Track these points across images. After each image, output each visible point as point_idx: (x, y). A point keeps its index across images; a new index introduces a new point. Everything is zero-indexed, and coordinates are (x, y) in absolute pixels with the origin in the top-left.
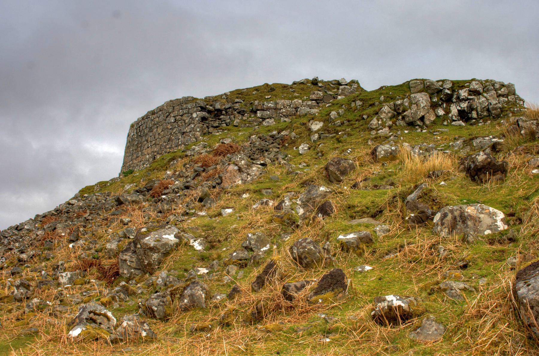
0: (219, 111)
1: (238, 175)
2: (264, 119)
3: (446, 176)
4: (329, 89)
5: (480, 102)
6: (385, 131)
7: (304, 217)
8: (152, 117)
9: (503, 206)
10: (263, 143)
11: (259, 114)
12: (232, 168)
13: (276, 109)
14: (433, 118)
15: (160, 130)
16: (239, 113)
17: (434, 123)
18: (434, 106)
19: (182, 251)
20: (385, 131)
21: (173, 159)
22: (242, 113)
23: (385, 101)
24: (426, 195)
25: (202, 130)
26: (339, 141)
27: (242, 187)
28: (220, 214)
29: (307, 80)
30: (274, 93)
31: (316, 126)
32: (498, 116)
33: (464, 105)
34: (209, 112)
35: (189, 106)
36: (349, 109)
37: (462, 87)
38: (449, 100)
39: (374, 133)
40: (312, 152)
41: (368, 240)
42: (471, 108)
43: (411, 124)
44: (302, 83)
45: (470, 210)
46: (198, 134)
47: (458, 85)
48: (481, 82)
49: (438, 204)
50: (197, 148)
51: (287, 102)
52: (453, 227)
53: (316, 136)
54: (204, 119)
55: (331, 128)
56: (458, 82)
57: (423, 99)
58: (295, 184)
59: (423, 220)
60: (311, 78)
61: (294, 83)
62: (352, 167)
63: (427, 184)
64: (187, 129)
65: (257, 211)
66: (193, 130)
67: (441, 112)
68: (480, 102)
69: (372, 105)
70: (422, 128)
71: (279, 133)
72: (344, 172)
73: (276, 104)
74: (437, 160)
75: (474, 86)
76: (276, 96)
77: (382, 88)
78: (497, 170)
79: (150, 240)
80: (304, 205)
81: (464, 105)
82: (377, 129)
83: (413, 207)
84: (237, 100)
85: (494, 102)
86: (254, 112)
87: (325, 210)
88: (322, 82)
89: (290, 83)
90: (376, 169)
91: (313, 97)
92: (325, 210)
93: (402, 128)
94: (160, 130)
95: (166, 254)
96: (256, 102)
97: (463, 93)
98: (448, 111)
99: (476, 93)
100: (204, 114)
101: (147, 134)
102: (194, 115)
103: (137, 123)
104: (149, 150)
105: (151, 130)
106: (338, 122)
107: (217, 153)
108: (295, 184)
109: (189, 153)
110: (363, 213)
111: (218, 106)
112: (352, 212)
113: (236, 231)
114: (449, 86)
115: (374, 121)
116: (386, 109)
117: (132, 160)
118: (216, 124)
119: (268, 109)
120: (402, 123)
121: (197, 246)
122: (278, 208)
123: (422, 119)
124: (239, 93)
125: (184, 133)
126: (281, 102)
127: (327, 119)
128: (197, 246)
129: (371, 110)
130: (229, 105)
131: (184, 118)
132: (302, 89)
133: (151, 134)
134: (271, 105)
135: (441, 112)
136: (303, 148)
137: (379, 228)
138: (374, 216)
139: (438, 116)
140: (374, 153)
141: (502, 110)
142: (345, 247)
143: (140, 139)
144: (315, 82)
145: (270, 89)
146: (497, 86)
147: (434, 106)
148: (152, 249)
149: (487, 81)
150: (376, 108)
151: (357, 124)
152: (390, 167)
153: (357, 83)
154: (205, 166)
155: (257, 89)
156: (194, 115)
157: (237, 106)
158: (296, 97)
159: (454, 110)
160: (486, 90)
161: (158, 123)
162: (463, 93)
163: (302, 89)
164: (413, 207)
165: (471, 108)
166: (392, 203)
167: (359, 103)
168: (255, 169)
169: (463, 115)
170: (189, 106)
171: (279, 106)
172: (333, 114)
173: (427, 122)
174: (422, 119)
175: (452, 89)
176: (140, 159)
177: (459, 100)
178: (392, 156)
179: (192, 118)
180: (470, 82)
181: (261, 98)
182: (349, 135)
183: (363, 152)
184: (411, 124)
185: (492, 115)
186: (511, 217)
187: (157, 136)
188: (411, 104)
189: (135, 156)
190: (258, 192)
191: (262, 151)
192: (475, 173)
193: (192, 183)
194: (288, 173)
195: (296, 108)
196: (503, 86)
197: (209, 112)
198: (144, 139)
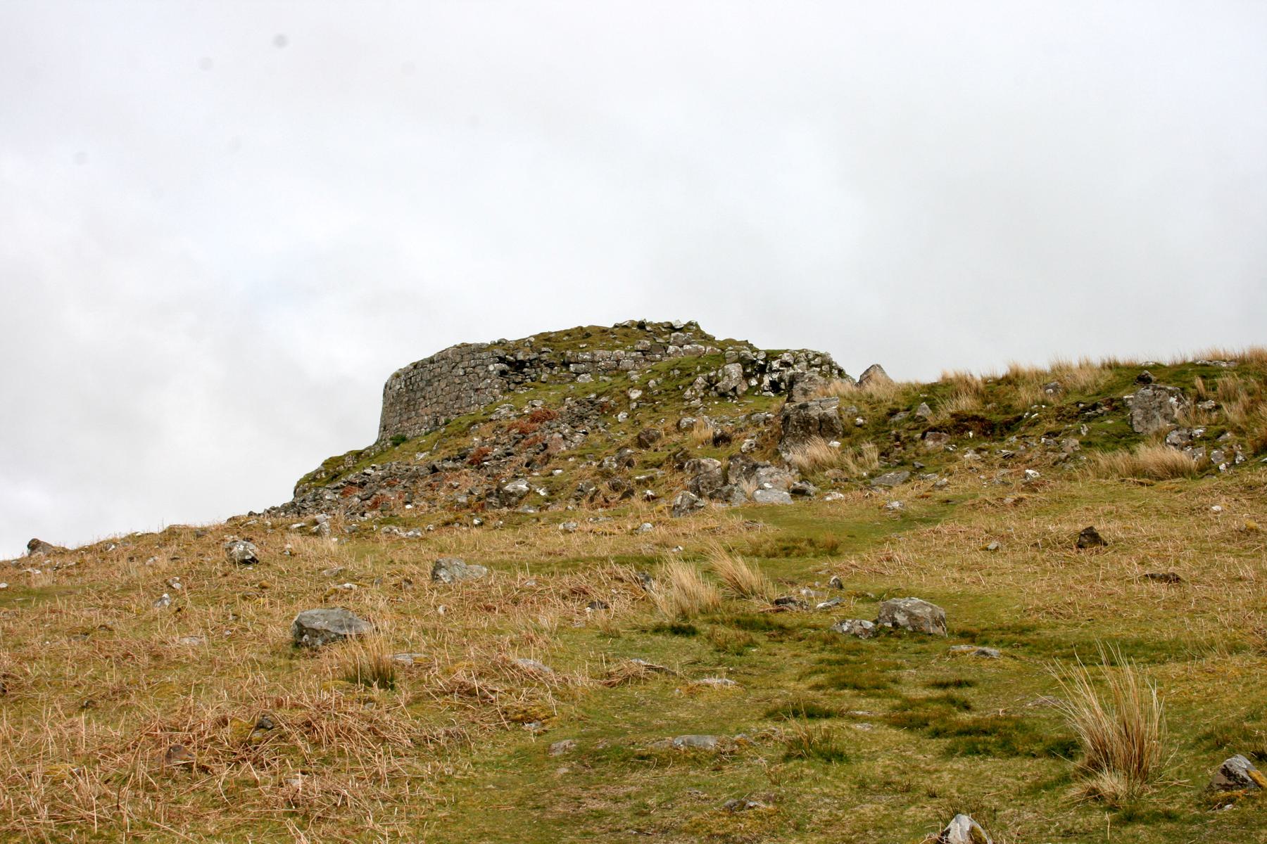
1: (562, 442)
2: (578, 374)
4: (659, 335)
6: (697, 402)
7: (617, 469)
8: (431, 367)
10: (582, 409)
12: (557, 435)
14: (745, 389)
15: (443, 384)
16: (547, 365)
17: (746, 393)
18: (747, 377)
19: (532, 496)
20: (697, 402)
21: (474, 423)
22: (551, 366)
23: (701, 372)
25: (501, 387)
26: (655, 411)
27: (568, 453)
28: (551, 474)
29: (633, 323)
30: (589, 340)
31: (635, 394)
33: (775, 376)
34: (509, 363)
35: (484, 355)
36: (667, 378)
37: (775, 358)
38: (762, 370)
39: (686, 403)
40: (630, 421)
41: (651, 479)
43: (723, 396)
44: (626, 326)
45: (703, 461)
46: (497, 391)
47: (771, 356)
48: (793, 353)
50: (503, 412)
51: (607, 353)
52: (693, 470)
53: (635, 405)
54: (503, 373)
55: (648, 398)
56: (773, 352)
57: (735, 370)
58: (613, 450)
60: (637, 320)
61: (616, 326)
64: (482, 385)
65: (584, 470)
67: (754, 382)
69: (689, 375)
70: (733, 398)
71: (597, 397)
72: (652, 440)
73: (593, 355)
75: (786, 357)
76: (592, 344)
79: (509, 488)
80: (617, 461)
81: (775, 376)
82: (689, 400)
84: (544, 349)
86: (566, 364)
87: (630, 464)
88: (650, 324)
89: (610, 325)
91: (639, 347)
92: (630, 464)
93: (714, 399)
94: (443, 384)
95: (521, 498)
96: (569, 353)
97: (775, 364)
98: (760, 381)
100: (504, 366)
101: (423, 389)
102: (491, 368)
103: (406, 372)
104: (429, 410)
105: (429, 383)
107: (534, 419)
108: (613, 450)
109: (493, 417)
110: (652, 466)
111: (520, 357)
112: (646, 465)
113: (569, 483)
114: (762, 356)
115: (688, 393)
116: (700, 380)
117: (400, 422)
119: (584, 361)
120: (714, 394)
121: (542, 493)
122: (600, 466)
123: (734, 389)
124: (545, 338)
125: (477, 390)
126: (599, 353)
127: (646, 389)
128: (542, 493)
129: (686, 381)
130: (535, 355)
131: (477, 370)
132: (626, 335)
133: (430, 389)
134: (587, 357)
136: (622, 416)
138: (1142, 643)
139: (750, 387)
140: (678, 424)
142: (639, 482)
143: (412, 394)
144: (642, 326)
145: (584, 335)
146: (811, 356)
147: (747, 377)
148: (512, 494)
150: (691, 379)
151: (673, 394)
153: (697, 325)
154: (523, 432)
155: (568, 333)
156: (491, 368)
157: (544, 356)
158: (618, 347)
159: (767, 380)
160: (797, 362)
161: (440, 375)
162: (775, 364)
163: (626, 335)
165: (781, 379)
166: (668, 459)
167: (677, 372)
168: (578, 438)
169: (775, 386)
171: (596, 359)
172: (652, 383)
173: (739, 393)
175: (766, 360)
176: (413, 421)
177: (772, 371)
180: (782, 352)
181: (574, 347)
182: (665, 405)
183: (670, 424)
187: (439, 392)
188: (724, 375)
189: (405, 417)
190: (583, 456)
191: (582, 418)
193: (513, 450)
194: (608, 441)
195: (618, 361)
196: (817, 355)
197: (509, 363)
198: (419, 394)
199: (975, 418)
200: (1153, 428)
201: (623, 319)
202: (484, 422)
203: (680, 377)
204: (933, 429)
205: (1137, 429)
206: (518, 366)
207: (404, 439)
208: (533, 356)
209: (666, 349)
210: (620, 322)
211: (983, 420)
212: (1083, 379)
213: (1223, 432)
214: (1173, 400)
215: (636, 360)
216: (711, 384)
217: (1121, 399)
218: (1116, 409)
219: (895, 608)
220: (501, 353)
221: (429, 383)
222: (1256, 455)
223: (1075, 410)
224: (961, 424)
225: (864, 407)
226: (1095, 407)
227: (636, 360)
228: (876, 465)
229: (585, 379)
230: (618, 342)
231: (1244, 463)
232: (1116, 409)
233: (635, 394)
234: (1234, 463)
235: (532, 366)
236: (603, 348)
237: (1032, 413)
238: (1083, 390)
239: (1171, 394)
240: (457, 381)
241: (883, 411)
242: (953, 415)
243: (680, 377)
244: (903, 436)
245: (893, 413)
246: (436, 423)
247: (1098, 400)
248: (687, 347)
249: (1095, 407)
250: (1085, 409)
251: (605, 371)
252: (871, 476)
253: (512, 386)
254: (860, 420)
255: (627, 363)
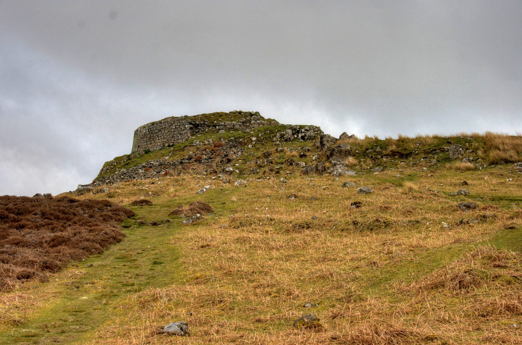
0: (198, 125)
2: (219, 130)
3: (296, 157)
5: (308, 133)
6: (278, 142)
9: (305, 162)
11: (217, 127)
12: (232, 152)
13: (225, 126)
15: (166, 131)
17: (293, 140)
18: (293, 134)
20: (278, 142)
21: (186, 146)
22: (209, 126)
23: (278, 132)
24: (292, 160)
25: (191, 133)
26: (263, 145)
29: (236, 112)
31: (254, 139)
32: (313, 139)
34: (193, 125)
35: (183, 122)
36: (265, 134)
38: (298, 132)
42: (305, 136)
46: (189, 135)
47: (301, 127)
49: (294, 161)
50: (197, 143)
51: (230, 123)
54: (191, 128)
55: (258, 140)
57: (290, 131)
59: (291, 164)
60: (238, 110)
61: (230, 113)
62: (271, 154)
63: (292, 158)
66: (186, 133)
67: (296, 136)
68: (308, 133)
69: (273, 133)
72: (269, 155)
73: (225, 123)
74: (294, 153)
75: (307, 128)
77: (274, 120)
78: (305, 156)
80: (267, 162)
81: (303, 134)
83: (289, 162)
85: (312, 134)
86: (215, 127)
88: (243, 112)
89: (228, 112)
90: (278, 154)
91: (241, 121)
93: (283, 142)
94: (166, 131)
96: (215, 122)
97: (303, 130)
98: (298, 136)
99: (307, 130)
100: (192, 126)
102: (187, 126)
104: (160, 141)
106: (262, 138)
110: (279, 163)
111: (197, 123)
115: (274, 139)
116: (278, 135)
118: (197, 131)
119: (221, 125)
123: (290, 138)
124: (205, 116)
126: (227, 122)
127: (257, 137)
131: (181, 127)
132: (235, 116)
133: (160, 133)
135: (296, 136)
136: (250, 146)
137: (283, 166)
140: (277, 150)
141: (315, 137)
143: (152, 135)
144: (240, 113)
145: (220, 115)
147: (293, 134)
149: (311, 126)
150: (275, 134)
151: (269, 139)
152: (282, 154)
155: (213, 114)
156: (187, 126)
157: (206, 123)
158: (233, 120)
159: (300, 135)
161: (165, 128)
162: (303, 130)
163: (235, 116)
164: (289, 162)
165: (305, 136)
166: (285, 162)
167: (269, 132)
169: (303, 137)
170: (183, 122)
171: (226, 124)
172: (260, 135)
174: (290, 138)
175: (300, 129)
177: (302, 132)
178: (282, 151)
179: (185, 127)
184: (286, 140)
185: (311, 138)
186: (306, 164)
187: (164, 134)
189: (149, 143)
192: (301, 156)
193: (211, 157)
195: (234, 126)
197: (193, 125)
198: (155, 135)
199: (398, 152)
200: (456, 157)
201: (233, 110)
202: (190, 146)
203: (270, 134)
204: (385, 155)
205: (451, 157)
206: (196, 126)
207: (149, 151)
208: (202, 122)
209: (251, 122)
210: (232, 111)
211: (400, 153)
212: (429, 141)
213: (479, 159)
214: (461, 149)
215: (240, 125)
216: (282, 136)
217: (443, 148)
218: (442, 151)
219: (461, 191)
220: (190, 121)
221: (160, 131)
222: (489, 165)
223: (429, 151)
224: (393, 154)
225: (358, 147)
226: (435, 150)
227: (240, 125)
228: (371, 165)
229: (222, 132)
230: (233, 119)
231: (486, 168)
232: (442, 151)
233: (254, 139)
234: (483, 167)
235: (201, 126)
236: (228, 120)
237: (415, 151)
238: (430, 145)
239: (460, 147)
240: (172, 130)
241: (364, 149)
242: (391, 151)
243: (270, 134)
244: (374, 157)
245: (367, 149)
246: (164, 146)
247: (436, 148)
248: (258, 121)
249: (435, 150)
250: (432, 151)
251: (230, 129)
252: (371, 168)
253: (194, 133)
254: (357, 151)
255: (237, 127)
